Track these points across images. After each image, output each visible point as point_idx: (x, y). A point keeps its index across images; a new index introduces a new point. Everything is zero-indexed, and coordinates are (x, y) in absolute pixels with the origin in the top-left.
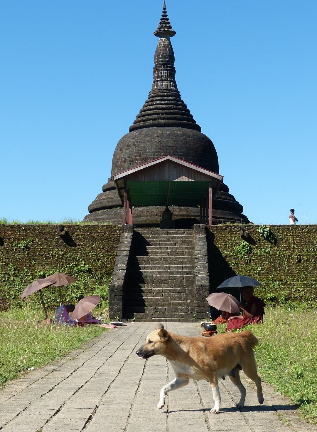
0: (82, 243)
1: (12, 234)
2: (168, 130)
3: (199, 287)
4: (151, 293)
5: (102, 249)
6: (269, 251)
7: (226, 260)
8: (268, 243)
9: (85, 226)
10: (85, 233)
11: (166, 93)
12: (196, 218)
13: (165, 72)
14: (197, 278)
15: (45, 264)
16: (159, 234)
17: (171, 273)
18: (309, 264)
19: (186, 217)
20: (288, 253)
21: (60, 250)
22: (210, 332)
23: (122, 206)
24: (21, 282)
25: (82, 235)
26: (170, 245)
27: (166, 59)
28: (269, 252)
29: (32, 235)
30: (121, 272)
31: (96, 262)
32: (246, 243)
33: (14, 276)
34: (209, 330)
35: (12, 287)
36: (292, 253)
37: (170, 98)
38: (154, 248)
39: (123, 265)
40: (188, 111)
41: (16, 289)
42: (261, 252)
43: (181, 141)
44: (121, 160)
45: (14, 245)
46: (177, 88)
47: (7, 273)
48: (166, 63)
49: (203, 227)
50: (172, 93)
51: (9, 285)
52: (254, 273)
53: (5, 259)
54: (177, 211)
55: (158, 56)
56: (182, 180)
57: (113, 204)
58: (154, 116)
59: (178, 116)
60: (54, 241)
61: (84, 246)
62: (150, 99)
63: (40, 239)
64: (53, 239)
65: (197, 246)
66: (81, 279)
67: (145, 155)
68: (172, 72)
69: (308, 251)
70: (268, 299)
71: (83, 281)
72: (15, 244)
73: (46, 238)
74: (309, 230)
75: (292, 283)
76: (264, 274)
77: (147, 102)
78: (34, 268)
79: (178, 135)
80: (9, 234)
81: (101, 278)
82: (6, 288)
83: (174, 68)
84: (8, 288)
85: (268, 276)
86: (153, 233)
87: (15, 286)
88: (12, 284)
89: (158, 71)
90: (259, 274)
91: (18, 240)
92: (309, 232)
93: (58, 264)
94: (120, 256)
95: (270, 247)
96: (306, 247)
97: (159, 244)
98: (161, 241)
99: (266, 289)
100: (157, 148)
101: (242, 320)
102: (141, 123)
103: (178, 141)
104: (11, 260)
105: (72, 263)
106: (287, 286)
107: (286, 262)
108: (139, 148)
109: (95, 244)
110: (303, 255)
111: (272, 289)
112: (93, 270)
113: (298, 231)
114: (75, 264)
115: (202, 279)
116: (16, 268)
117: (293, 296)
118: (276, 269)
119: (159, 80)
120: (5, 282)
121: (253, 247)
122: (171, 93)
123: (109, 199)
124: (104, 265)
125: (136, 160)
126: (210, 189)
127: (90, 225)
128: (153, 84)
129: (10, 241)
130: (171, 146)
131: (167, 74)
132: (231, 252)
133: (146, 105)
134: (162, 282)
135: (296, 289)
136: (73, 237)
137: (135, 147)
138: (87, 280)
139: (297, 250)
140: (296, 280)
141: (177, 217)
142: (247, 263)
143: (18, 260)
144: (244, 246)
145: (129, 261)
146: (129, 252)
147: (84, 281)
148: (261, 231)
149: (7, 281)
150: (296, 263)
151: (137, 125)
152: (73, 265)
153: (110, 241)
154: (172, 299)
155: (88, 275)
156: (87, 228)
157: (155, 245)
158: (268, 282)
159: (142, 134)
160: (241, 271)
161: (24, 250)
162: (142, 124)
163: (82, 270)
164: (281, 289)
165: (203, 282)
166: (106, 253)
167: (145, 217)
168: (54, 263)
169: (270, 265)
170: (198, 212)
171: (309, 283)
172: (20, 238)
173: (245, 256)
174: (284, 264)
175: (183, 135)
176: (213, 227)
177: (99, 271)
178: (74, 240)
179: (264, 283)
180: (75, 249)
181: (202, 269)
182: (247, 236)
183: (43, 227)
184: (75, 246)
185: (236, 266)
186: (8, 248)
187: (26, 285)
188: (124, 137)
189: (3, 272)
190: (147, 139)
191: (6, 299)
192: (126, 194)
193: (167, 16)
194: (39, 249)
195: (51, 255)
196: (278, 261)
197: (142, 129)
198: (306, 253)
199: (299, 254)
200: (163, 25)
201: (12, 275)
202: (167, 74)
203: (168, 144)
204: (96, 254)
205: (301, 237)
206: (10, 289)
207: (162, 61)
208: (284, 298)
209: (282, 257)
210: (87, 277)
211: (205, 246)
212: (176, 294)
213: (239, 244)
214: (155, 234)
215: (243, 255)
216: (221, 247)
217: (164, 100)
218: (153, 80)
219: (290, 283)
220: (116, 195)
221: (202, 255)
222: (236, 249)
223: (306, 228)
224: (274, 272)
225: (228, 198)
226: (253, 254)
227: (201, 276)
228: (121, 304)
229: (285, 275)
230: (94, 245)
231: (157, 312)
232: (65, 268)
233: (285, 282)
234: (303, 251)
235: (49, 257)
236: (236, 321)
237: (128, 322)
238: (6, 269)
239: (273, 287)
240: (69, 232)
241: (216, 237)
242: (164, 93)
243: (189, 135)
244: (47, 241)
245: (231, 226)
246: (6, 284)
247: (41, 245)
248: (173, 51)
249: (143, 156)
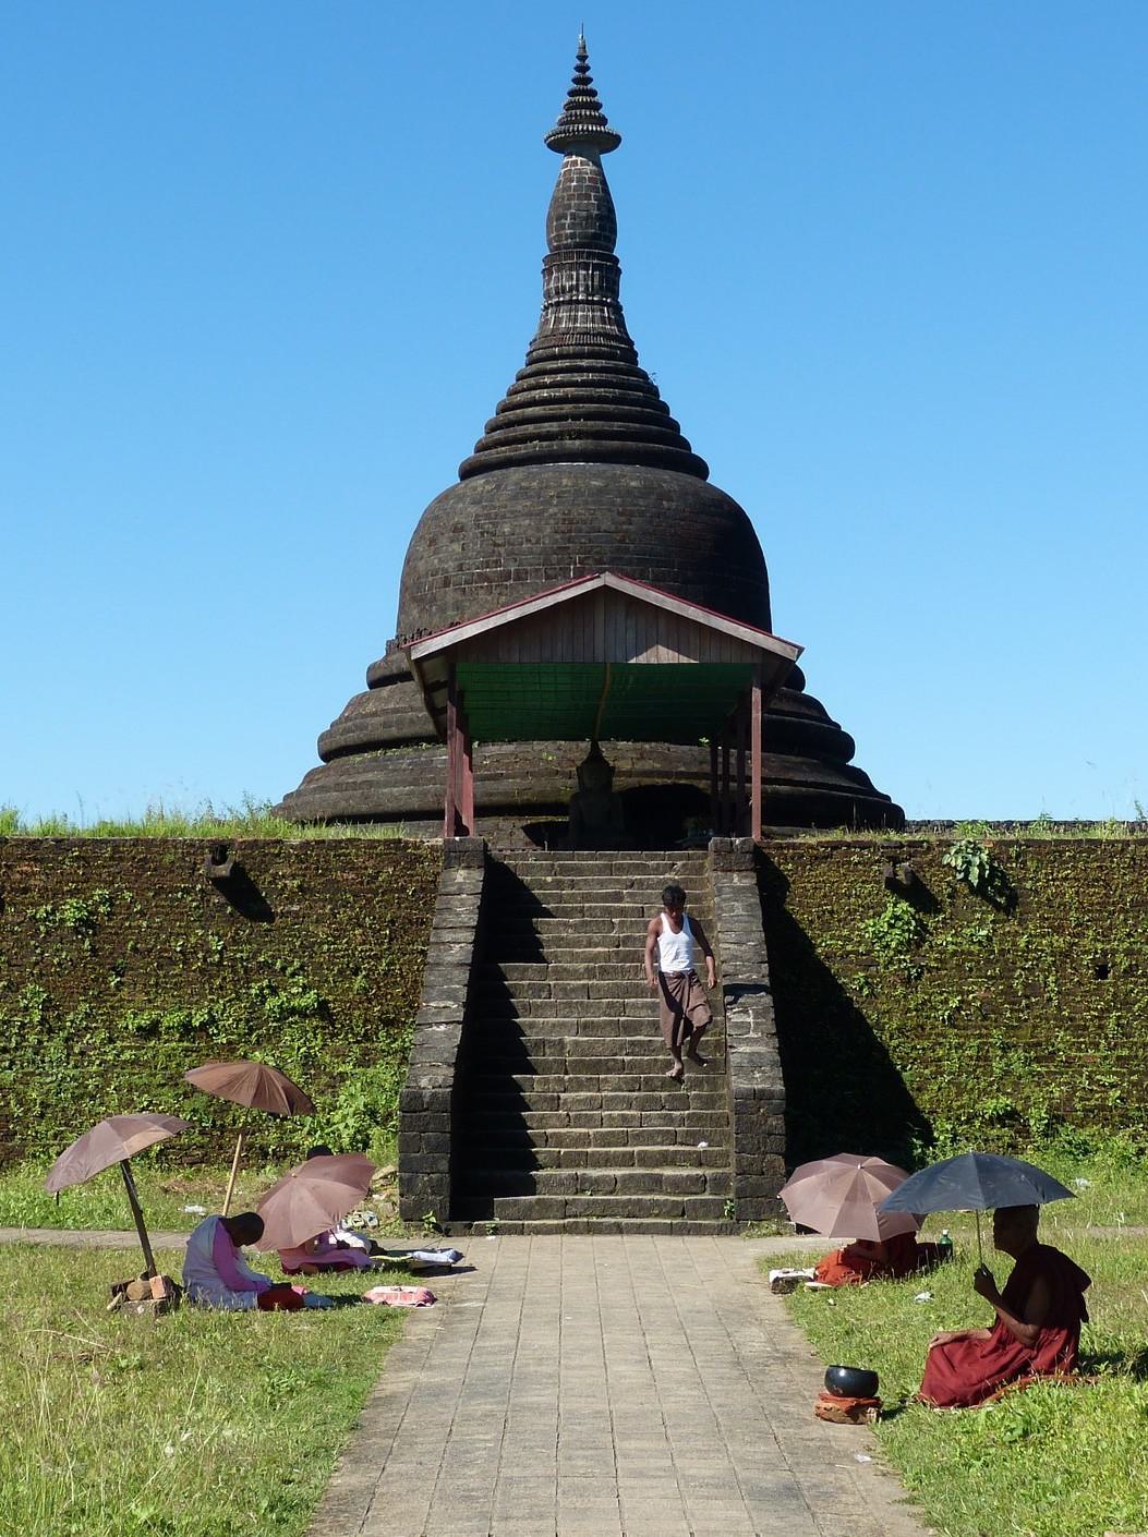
0: (296, 908)
1: (34, 874)
2: (594, 475)
3: (746, 1099)
4: (561, 1116)
5: (370, 928)
6: (987, 936)
7: (829, 970)
8: (984, 908)
9: (308, 842)
10: (306, 868)
11: (587, 345)
12: (695, 783)
13: (584, 272)
15: (157, 984)
16: (579, 871)
17: (630, 1028)
18: (1135, 983)
19: (659, 781)
20: (1060, 942)
21: (212, 934)
22: (850, 1402)
23: (439, 738)
24: (68, 1055)
25: (294, 877)
26: (622, 912)
27: (587, 228)
28: (989, 939)
29: (109, 876)
30: (444, 1032)
31: (346, 978)
32: (904, 905)
33: (41, 1032)
34: (846, 1395)
35: (33, 1074)
36: (1075, 944)
37: (602, 363)
38: (565, 924)
39: (449, 1003)
40: (664, 408)
41: (48, 1080)
42: (959, 940)
43: (642, 514)
44: (431, 579)
45: (42, 914)
46: (625, 329)
47: (16, 1019)
48: (588, 244)
49: (746, 848)
50: (607, 346)
51: (21, 1066)
52: (935, 1017)
53: (10, 965)
54: (629, 758)
55: (559, 218)
56: (653, 661)
57: (404, 730)
58: (546, 424)
59: (628, 427)
60: (192, 901)
61: (304, 917)
62: (535, 367)
63: (140, 892)
64: (188, 894)
65: (726, 922)
66: (293, 1040)
67: (516, 560)
68: (610, 276)
69: (1133, 936)
70: (987, 1116)
71: (299, 1048)
72: (46, 912)
73: (162, 888)
74: (1133, 859)
75: (1073, 1054)
76: (970, 1020)
77: (520, 378)
78: (118, 1001)
79: (629, 492)
80: (21, 873)
81: (367, 1037)
82: (10, 1075)
83: (616, 260)
84: (20, 1075)
85: (984, 1031)
86: (560, 865)
87: (44, 1068)
88: (34, 1062)
89: (560, 268)
90: (952, 1021)
91: (55, 895)
92: (1135, 864)
93: (207, 986)
94: (438, 964)
95: (993, 922)
96: (1125, 920)
97: (582, 910)
98: (587, 898)
99: (978, 1078)
100: (558, 536)
102: (503, 448)
103: (632, 514)
104: (31, 972)
105: (256, 981)
106: (1055, 1067)
107: (1051, 979)
108: (495, 535)
109: (345, 912)
110: (1114, 952)
111: (1001, 1079)
112: (335, 1008)
113: (1096, 861)
114: (268, 987)
115: (754, 1063)
116: (48, 1000)
117: (1078, 1106)
118: (1014, 1003)
119: (563, 302)
120: (7, 1055)
121: (931, 923)
122: (604, 346)
123: (390, 716)
124: (379, 988)
125: (483, 577)
126: (756, 694)
127: (323, 841)
128: (544, 313)
129: (26, 901)
130: (605, 531)
131: (593, 281)
132: (848, 939)
133: (520, 388)
134: (596, 1067)
135: (1089, 1077)
136: (264, 883)
137: (482, 534)
138: (313, 1044)
139: (1091, 933)
140: (1091, 1043)
141: (630, 780)
142: (907, 981)
143: (56, 971)
144: (897, 918)
145: (471, 985)
146: (470, 947)
147: (302, 1050)
148: (960, 862)
149: (16, 1049)
150: (1090, 983)
152: (263, 989)
153: (398, 898)
154: (639, 1138)
155: (317, 1027)
156: (312, 851)
157: (567, 913)
158: (988, 1051)
159: (505, 489)
160: (888, 1012)
161: (79, 933)
162: (504, 452)
163: (294, 1008)
164: (1036, 1079)
165: (758, 1075)
166: (383, 943)
167: (518, 780)
168: (190, 983)
169: (992, 989)
170: (701, 763)
171: (1136, 1056)
172: (65, 888)
173: (902, 957)
174: (1046, 985)
175: (646, 491)
176: (782, 848)
177: (357, 1013)
178: (264, 895)
179: (971, 1058)
180: (270, 930)
181: (751, 1020)
182: (907, 879)
183: (148, 850)
184: (270, 918)
185: (866, 991)
186: (19, 924)
187: (86, 1064)
188: (443, 498)
190: (523, 505)
192: (454, 709)
193: (590, 80)
194: (135, 928)
195: (181, 951)
196: (1021, 975)
197: (504, 471)
198: (1126, 945)
199: (1099, 946)
200: (573, 112)
201: (33, 1028)
202: (593, 281)
203: (596, 524)
204: (346, 950)
205: (1107, 885)
206: (25, 1079)
207: (572, 236)
208: (1046, 1113)
209: (1037, 959)
210: (315, 1034)
211: (757, 925)
212: (655, 1121)
213: (879, 909)
214: (565, 870)
215: (892, 953)
216: (812, 922)
217: (580, 370)
218: (543, 302)
219: (1068, 1057)
220: (415, 700)
221: (748, 961)
222: (866, 928)
223: (1122, 850)
224: (1008, 1015)
225: (804, 710)
226: (931, 947)
227: (748, 1049)
228: (444, 1165)
229: (1047, 1026)
230: (339, 913)
231: (583, 1191)
232: (233, 999)
233: (1050, 1053)
234: (1113, 937)
235: (170, 958)
237: (472, 1235)
238: (12, 1006)
239: (1007, 1073)
240: (248, 867)
241: (794, 882)
242: (579, 344)
243: (670, 491)
244: (166, 900)
245: (849, 845)
246: (12, 1063)
247: (142, 913)
248: (610, 202)
249: (509, 565)
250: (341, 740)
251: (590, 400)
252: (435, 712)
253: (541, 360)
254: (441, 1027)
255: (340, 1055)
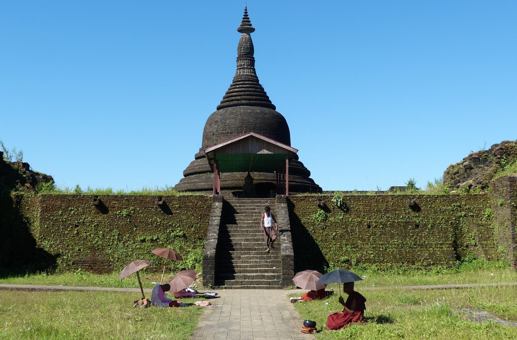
2: (249, 109)
4: (241, 261)
14: (282, 247)
16: (245, 203)
20: (359, 220)
22: (309, 329)
23: (212, 171)
26: (255, 213)
28: (342, 219)
32: (322, 211)
34: (309, 327)
40: (265, 93)
43: (260, 118)
45: (118, 213)
48: (247, 54)
54: (257, 176)
56: (263, 153)
62: (235, 83)
63: (141, 208)
77: (231, 86)
79: (257, 113)
81: (195, 242)
82: (110, 251)
90: (333, 239)
91: (121, 208)
97: (246, 212)
98: (247, 209)
101: (342, 316)
110: (372, 222)
115: (287, 248)
116: (119, 233)
125: (222, 133)
126: (287, 161)
134: (249, 249)
142: (323, 229)
144: (321, 214)
151: (223, 104)
157: (242, 213)
162: (227, 103)
175: (261, 113)
184: (172, 214)
189: (108, 237)
191: (110, 261)
206: (114, 252)
207: (244, 52)
211: (287, 216)
214: (242, 203)
218: (236, 68)
225: (298, 165)
228: (213, 273)
236: (335, 317)
239: (347, 251)
250: (189, 172)
251: (248, 91)
252: (211, 165)
253: (236, 82)
254: (212, 239)
255: (189, 246)
